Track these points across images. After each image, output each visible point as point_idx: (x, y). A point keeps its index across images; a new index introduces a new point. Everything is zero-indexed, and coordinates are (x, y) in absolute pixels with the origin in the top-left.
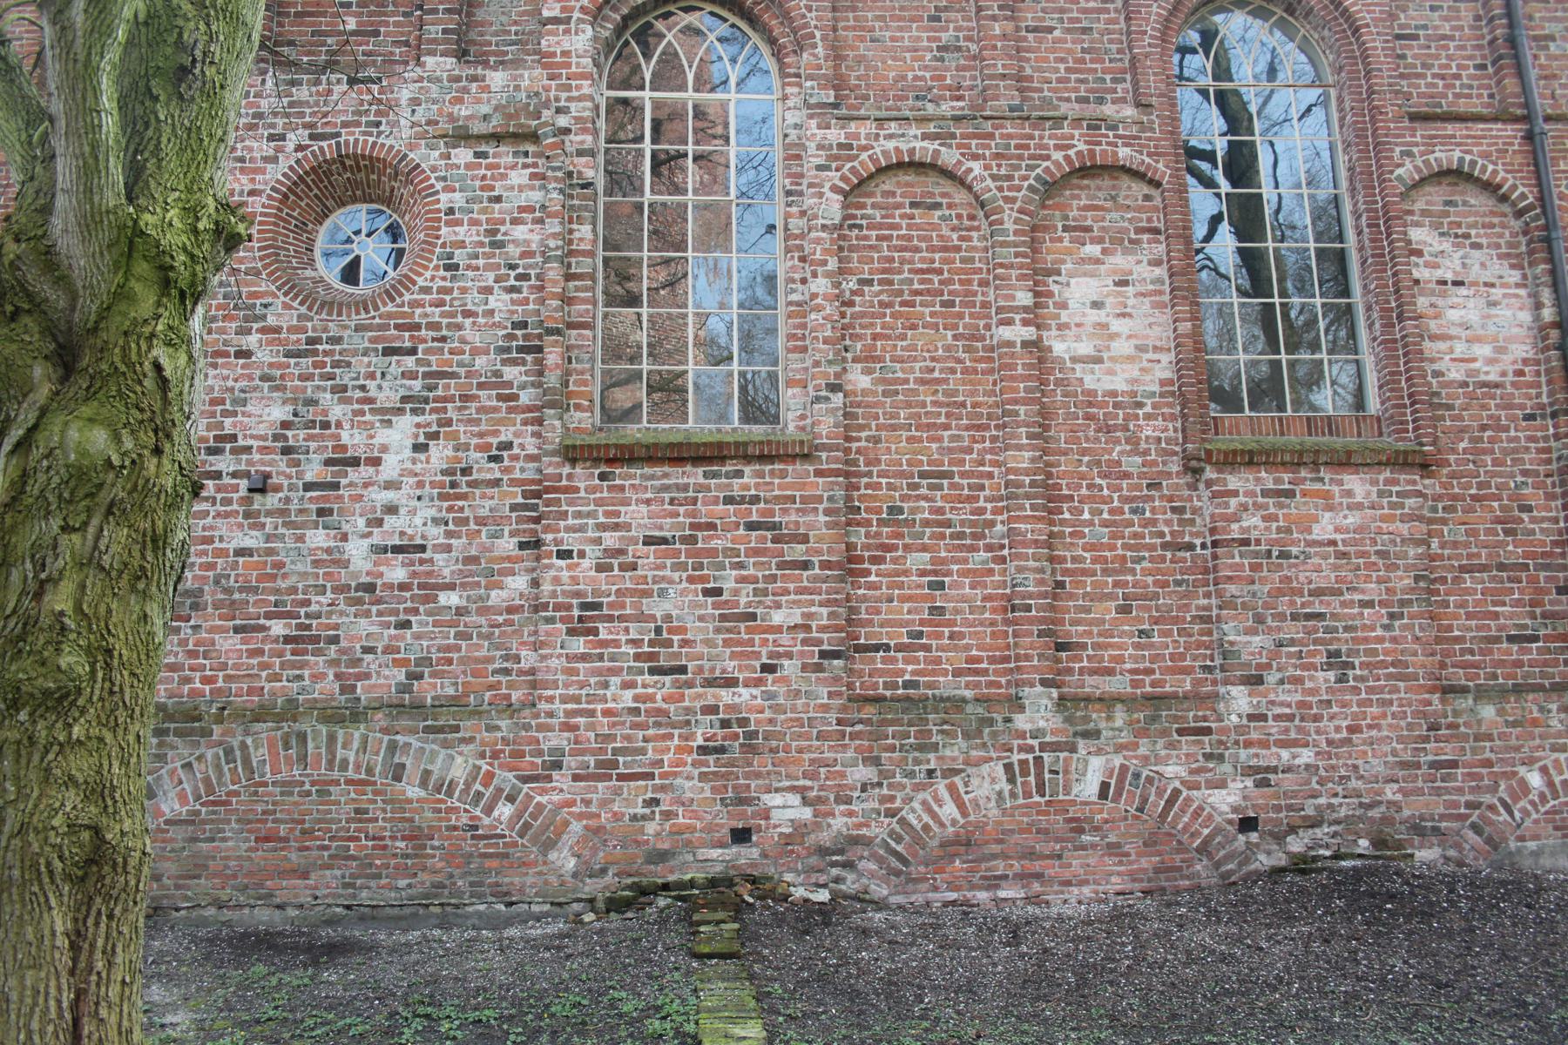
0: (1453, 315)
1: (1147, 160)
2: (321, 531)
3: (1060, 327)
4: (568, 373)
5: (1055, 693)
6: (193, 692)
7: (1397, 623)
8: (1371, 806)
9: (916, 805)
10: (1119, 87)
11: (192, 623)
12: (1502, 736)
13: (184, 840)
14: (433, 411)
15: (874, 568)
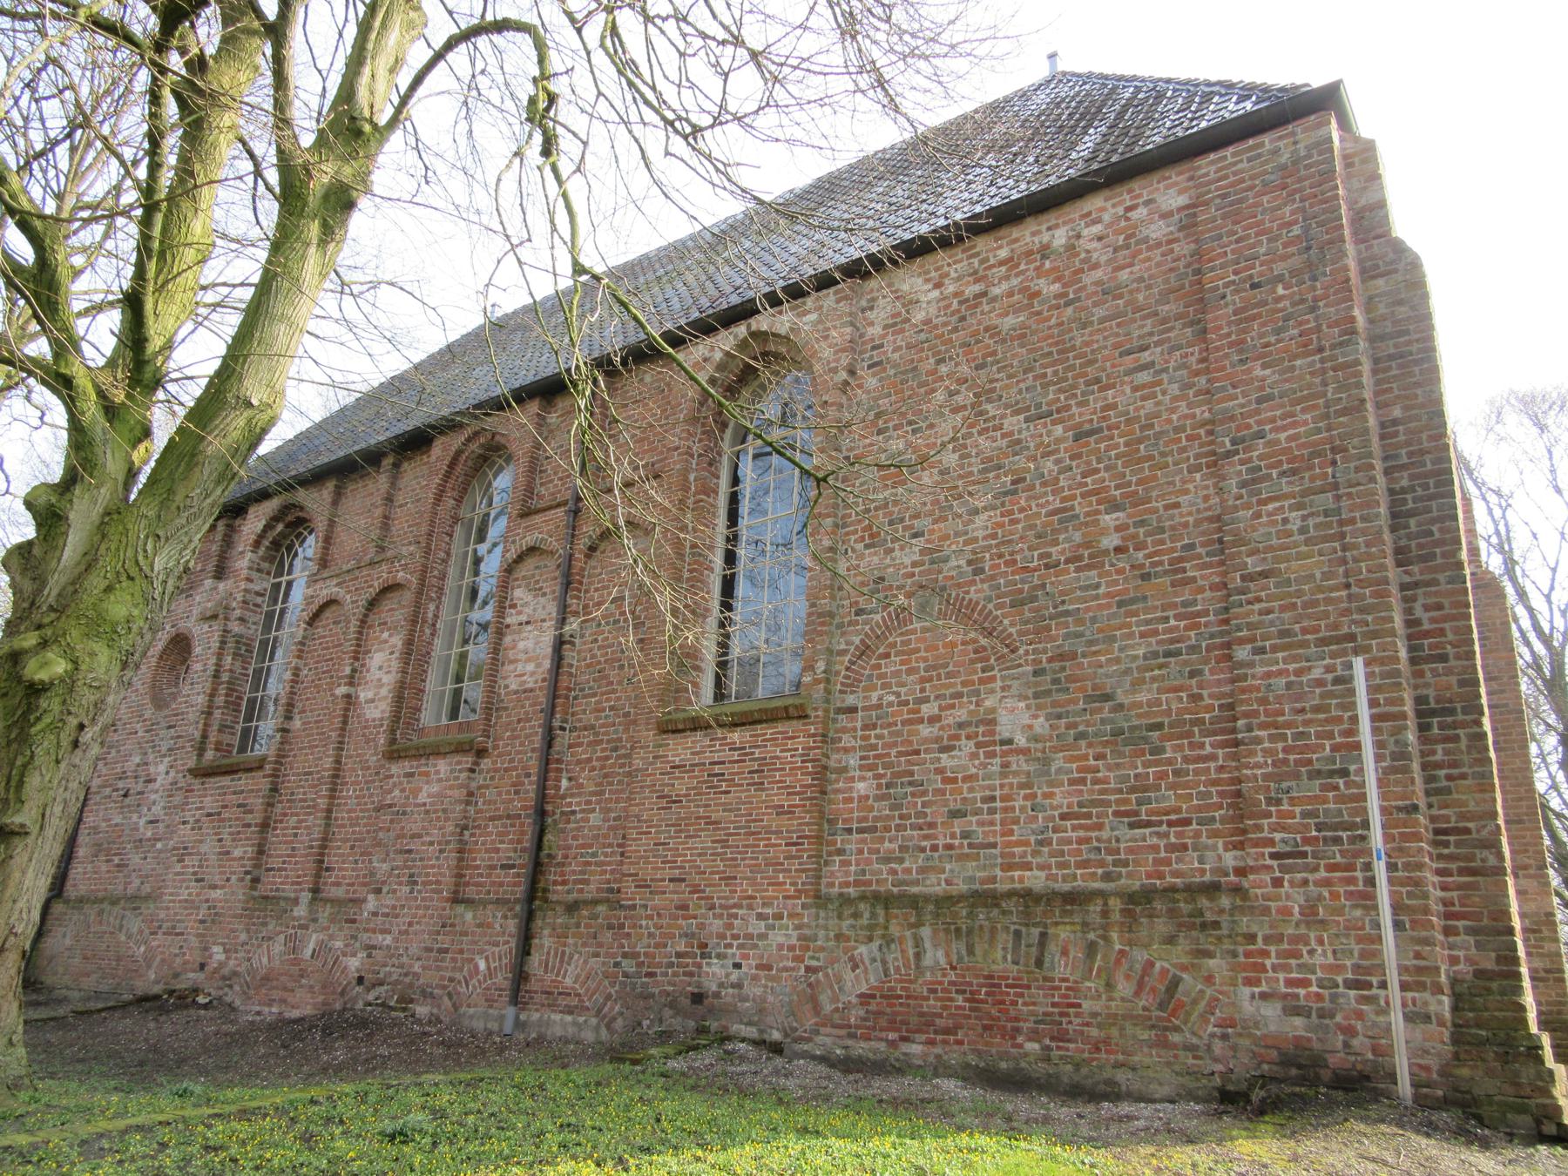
0: (521, 645)
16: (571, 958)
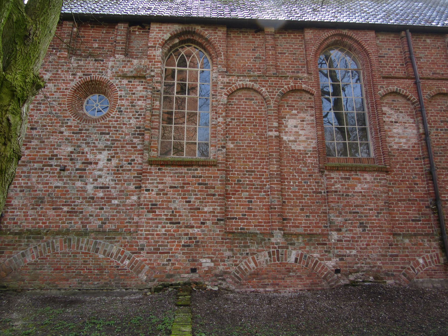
1: (310, 88)
2: (80, 182)
3: (285, 132)
4: (151, 141)
5: (282, 232)
6: (40, 227)
7: (380, 215)
8: (373, 267)
9: (243, 263)
10: (303, 69)
11: (41, 207)
12: (411, 248)
13: (32, 269)
14: (113, 150)
15: (233, 196)
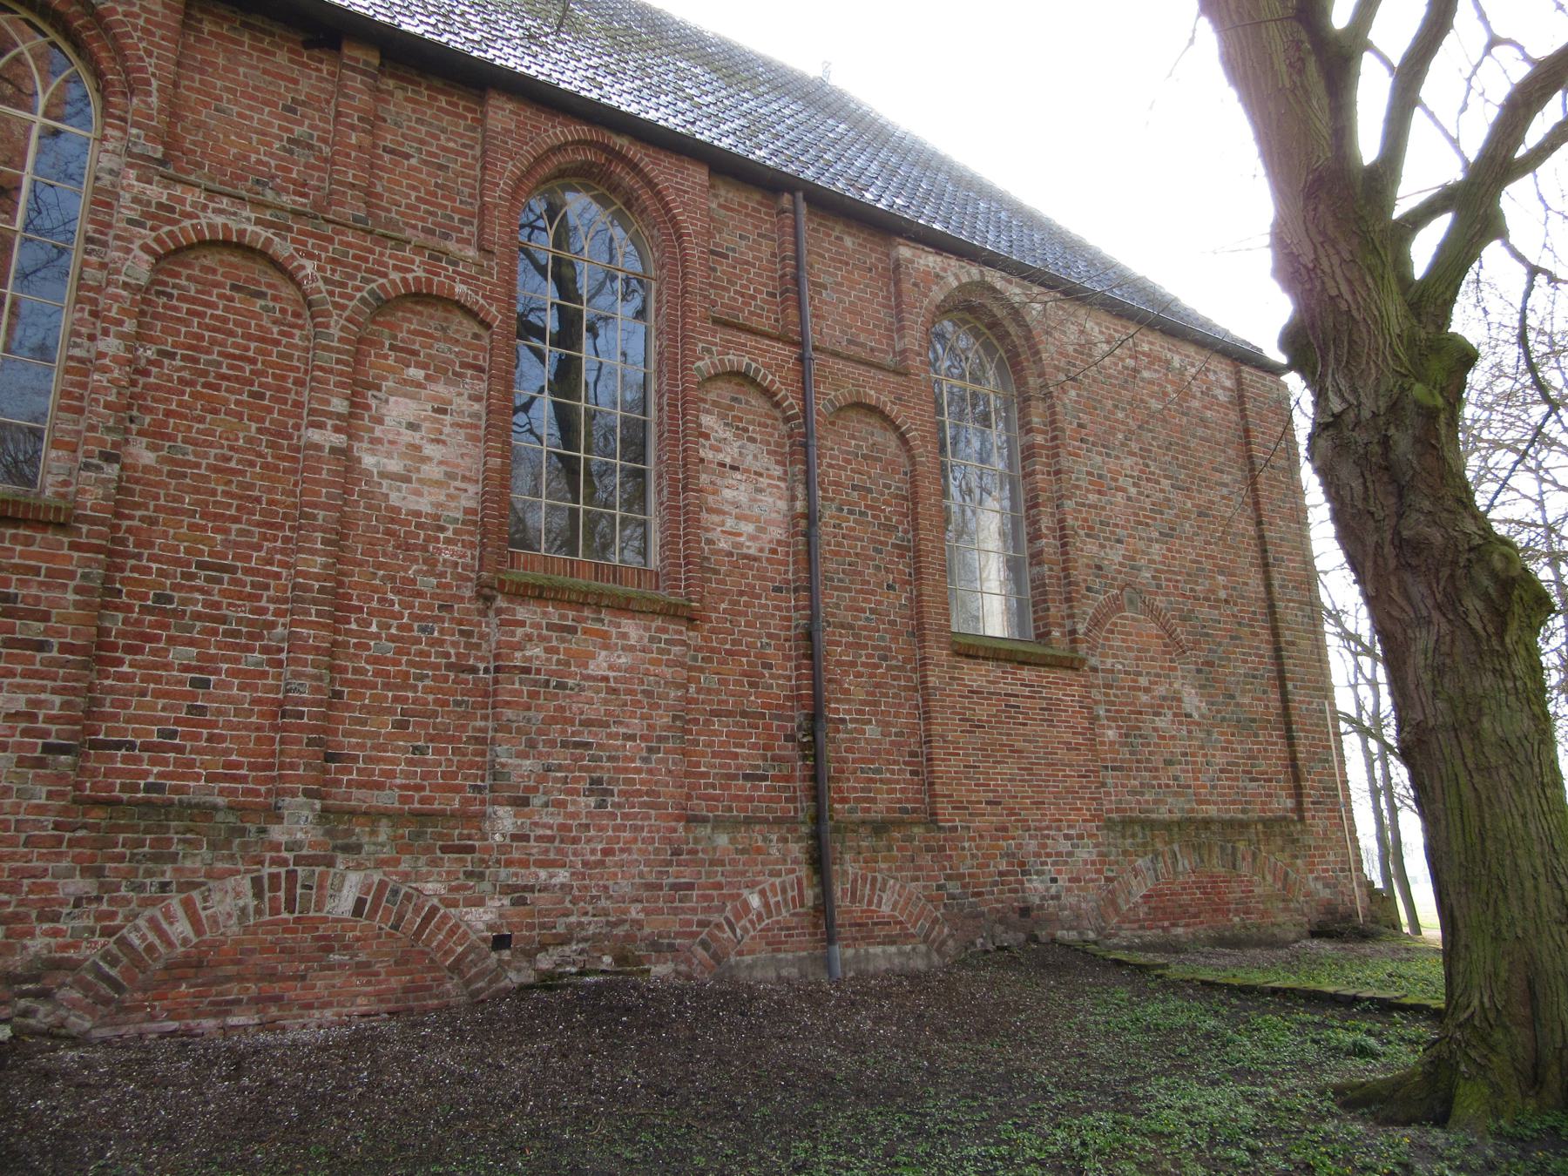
16: (885, 883)
